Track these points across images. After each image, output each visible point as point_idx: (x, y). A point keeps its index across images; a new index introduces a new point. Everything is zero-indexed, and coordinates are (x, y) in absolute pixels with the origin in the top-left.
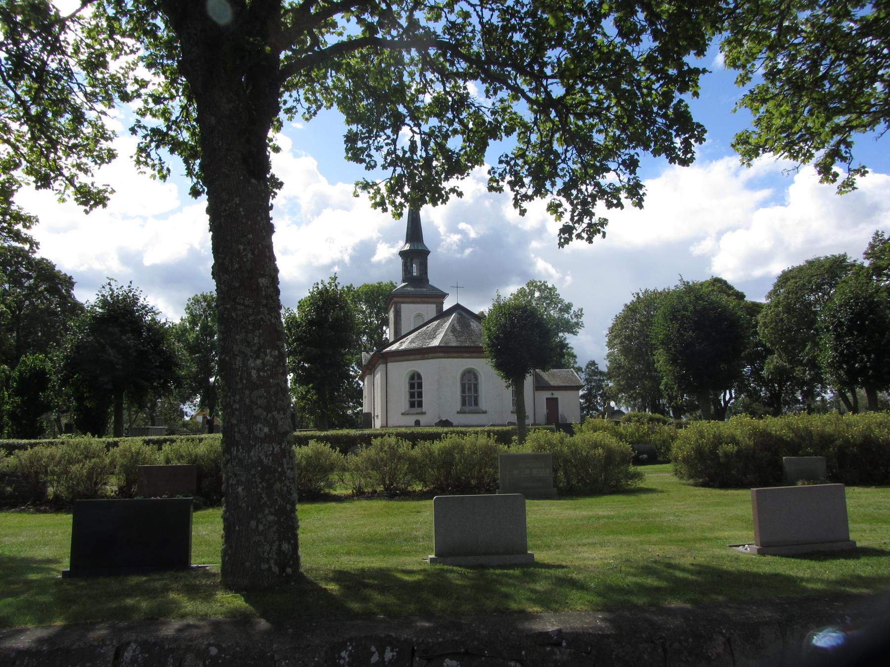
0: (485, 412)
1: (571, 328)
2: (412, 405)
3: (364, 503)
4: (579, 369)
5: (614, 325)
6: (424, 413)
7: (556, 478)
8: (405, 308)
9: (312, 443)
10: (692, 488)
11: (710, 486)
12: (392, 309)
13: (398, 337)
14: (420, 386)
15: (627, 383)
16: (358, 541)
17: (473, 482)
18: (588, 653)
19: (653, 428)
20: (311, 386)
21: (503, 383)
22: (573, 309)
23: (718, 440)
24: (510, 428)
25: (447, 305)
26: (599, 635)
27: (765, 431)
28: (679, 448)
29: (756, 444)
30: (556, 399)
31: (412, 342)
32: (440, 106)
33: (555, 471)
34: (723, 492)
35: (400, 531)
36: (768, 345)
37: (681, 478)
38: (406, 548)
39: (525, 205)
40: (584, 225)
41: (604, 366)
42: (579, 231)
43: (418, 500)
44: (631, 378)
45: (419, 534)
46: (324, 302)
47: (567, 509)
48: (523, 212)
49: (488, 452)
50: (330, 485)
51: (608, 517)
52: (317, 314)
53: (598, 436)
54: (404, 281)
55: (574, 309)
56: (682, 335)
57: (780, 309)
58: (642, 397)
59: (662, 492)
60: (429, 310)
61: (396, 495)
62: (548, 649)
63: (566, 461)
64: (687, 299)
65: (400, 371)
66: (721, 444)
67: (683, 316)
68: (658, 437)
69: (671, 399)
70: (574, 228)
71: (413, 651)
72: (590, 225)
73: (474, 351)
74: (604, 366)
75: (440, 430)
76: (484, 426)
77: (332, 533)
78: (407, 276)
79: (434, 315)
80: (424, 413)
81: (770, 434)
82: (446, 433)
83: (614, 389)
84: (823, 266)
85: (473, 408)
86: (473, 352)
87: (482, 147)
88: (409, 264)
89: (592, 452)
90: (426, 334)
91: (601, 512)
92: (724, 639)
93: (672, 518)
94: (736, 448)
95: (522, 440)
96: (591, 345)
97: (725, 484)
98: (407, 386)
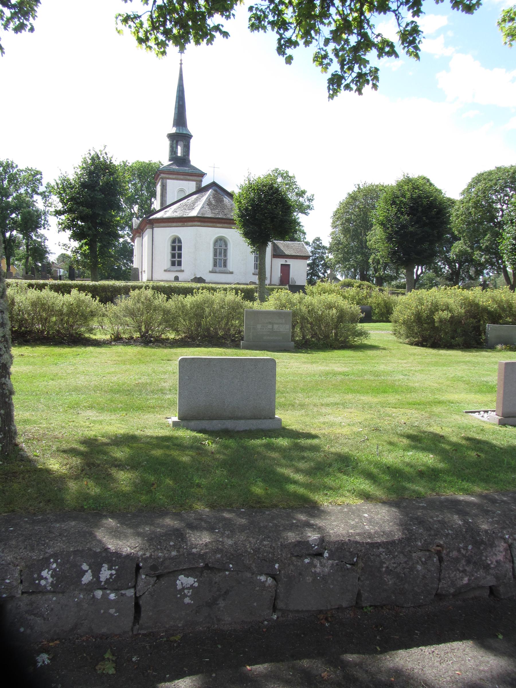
0: (232, 273)
1: (303, 209)
2: (173, 264)
3: (120, 349)
4: (307, 243)
5: (338, 209)
6: (183, 271)
9: (74, 292)
10: (409, 346)
11: (423, 346)
12: (160, 184)
13: (164, 207)
14: (180, 248)
15: (343, 257)
17: (221, 333)
18: (353, 564)
19: (370, 293)
22: (306, 194)
23: (435, 308)
24: (252, 286)
25: (206, 182)
26: (367, 543)
27: (473, 301)
28: (400, 312)
29: (465, 313)
30: (289, 266)
33: (293, 327)
36: (456, 233)
37: (399, 337)
38: (152, 403)
39: (289, 51)
40: (354, 75)
41: (326, 242)
42: (348, 81)
43: (170, 348)
44: (348, 253)
45: (166, 385)
46: (96, 168)
48: (289, 60)
49: (235, 308)
52: (89, 178)
53: (332, 298)
54: (170, 160)
55: (308, 194)
56: (399, 218)
57: (470, 204)
58: (354, 267)
59: (384, 349)
60: (191, 186)
61: (151, 342)
62: (307, 561)
63: (303, 318)
64: (406, 187)
65: (164, 235)
66: (437, 310)
67: (401, 201)
68: (374, 300)
69: (376, 270)
71: (138, 568)
72: (360, 76)
73: (227, 222)
74: (326, 242)
75: (194, 285)
76: (231, 284)
77: (81, 381)
78: (173, 157)
79: (194, 190)
80: (183, 271)
81: (477, 305)
82: (198, 289)
83: (333, 261)
84: (508, 172)
85: (222, 269)
86: (224, 223)
88: (175, 145)
90: (186, 205)
91: (337, 368)
92: (505, 545)
94: (450, 315)
95: (263, 299)
96: (318, 226)
97: (435, 345)
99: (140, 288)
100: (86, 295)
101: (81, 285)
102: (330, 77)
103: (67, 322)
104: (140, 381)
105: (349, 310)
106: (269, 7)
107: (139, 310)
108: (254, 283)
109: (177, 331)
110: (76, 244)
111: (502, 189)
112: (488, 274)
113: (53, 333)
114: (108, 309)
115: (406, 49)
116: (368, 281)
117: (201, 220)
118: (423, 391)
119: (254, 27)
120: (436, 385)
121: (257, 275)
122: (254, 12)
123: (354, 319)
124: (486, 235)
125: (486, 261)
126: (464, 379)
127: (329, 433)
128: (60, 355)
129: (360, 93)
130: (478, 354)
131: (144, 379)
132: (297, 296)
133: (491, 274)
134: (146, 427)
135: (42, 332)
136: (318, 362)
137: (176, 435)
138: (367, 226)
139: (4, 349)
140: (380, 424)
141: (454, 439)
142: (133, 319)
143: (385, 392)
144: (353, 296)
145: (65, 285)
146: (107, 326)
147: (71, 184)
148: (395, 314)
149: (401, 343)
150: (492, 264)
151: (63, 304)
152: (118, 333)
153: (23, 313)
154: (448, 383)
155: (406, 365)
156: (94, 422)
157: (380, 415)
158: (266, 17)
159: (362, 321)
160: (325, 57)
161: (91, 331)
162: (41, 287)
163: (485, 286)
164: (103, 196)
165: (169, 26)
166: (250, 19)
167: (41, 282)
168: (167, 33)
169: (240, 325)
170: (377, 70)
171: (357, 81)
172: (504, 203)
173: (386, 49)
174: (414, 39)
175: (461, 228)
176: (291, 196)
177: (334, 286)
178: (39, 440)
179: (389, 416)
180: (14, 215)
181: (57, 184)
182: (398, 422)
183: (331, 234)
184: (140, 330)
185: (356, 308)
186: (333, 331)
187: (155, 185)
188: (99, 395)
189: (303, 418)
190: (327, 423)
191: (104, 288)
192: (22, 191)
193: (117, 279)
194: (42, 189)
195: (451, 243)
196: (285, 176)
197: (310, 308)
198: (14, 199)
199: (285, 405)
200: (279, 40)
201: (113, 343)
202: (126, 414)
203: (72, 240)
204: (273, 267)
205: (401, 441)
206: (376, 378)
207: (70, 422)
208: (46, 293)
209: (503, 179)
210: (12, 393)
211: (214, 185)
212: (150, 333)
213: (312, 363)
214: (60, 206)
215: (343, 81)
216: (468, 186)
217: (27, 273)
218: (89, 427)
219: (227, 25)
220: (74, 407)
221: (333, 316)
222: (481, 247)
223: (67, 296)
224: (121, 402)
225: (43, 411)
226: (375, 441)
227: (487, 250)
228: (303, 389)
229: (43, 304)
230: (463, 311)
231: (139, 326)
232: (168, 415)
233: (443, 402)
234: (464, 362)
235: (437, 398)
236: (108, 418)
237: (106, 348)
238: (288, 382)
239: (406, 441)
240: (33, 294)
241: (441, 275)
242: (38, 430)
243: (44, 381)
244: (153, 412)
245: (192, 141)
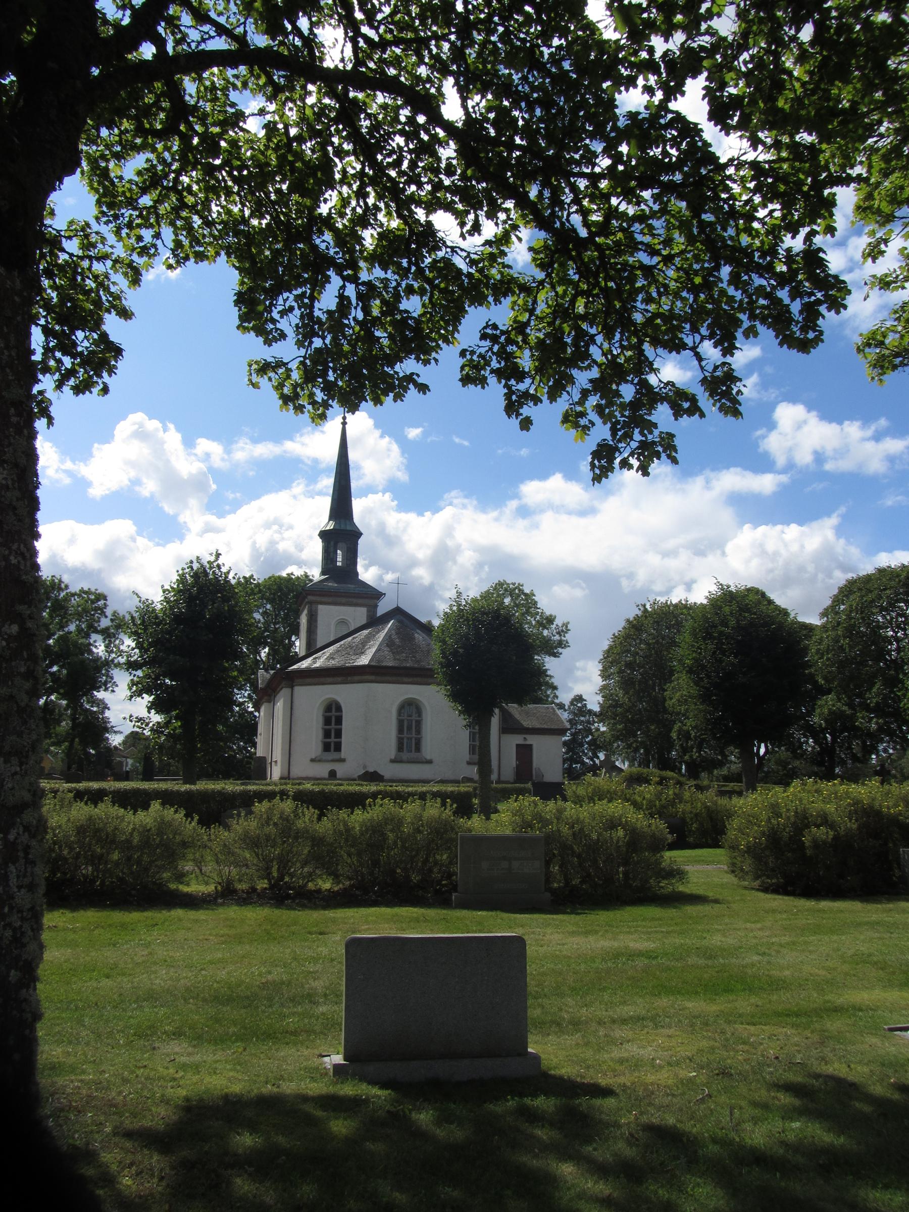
0: (430, 762)
1: (552, 648)
2: (326, 748)
3: (233, 912)
4: (561, 706)
6: (343, 760)
7: (548, 878)
8: (324, 611)
9: (155, 806)
10: (761, 895)
11: (787, 893)
12: (305, 612)
13: (312, 650)
14: (339, 720)
16: (205, 1000)
17: (415, 878)
20: (174, 713)
21: (461, 721)
23: (803, 821)
25: (383, 607)
27: (871, 807)
28: (740, 830)
29: (859, 828)
31: (331, 657)
32: (392, 249)
33: (548, 863)
34: (810, 904)
35: (285, 977)
38: (291, 1022)
40: (634, 445)
41: (594, 703)
46: (201, 589)
47: (573, 933)
48: (526, 424)
49: (441, 834)
50: (180, 877)
51: (650, 955)
53: (616, 808)
55: (559, 622)
59: (716, 901)
61: (288, 897)
64: (727, 610)
65: (311, 700)
66: (808, 826)
67: (721, 633)
68: (688, 808)
69: (685, 750)
70: (617, 449)
73: (421, 675)
74: (594, 703)
77: (161, 978)
79: (364, 621)
80: (343, 760)
81: (878, 813)
85: (413, 755)
87: (455, 315)
88: (332, 549)
89: (607, 834)
90: (351, 647)
93: (756, 958)
94: (831, 833)
95: (488, 811)
96: (580, 678)
97: (810, 892)
98: (321, 720)
99: (270, 796)
100: (176, 812)
101: (166, 790)
102: (595, 448)
103: (139, 862)
104: (270, 977)
105: (646, 829)
106: (491, 349)
107: (268, 838)
108: (470, 780)
109: (336, 876)
110: (156, 718)
111: (892, 605)
112: (885, 751)
113: (112, 882)
114: (213, 837)
115: (718, 405)
116: (672, 770)
117: (375, 673)
118: (800, 985)
119: (466, 380)
120: (822, 972)
121: (474, 764)
122: (468, 357)
123: (657, 845)
124: (874, 684)
125: (880, 729)
126: (875, 959)
127: (633, 1084)
128: (123, 926)
129: (646, 473)
130: (891, 906)
131: (278, 974)
132: (551, 806)
133: (891, 751)
134: (282, 1078)
135: (93, 881)
136: (596, 932)
137: (342, 1093)
138: (665, 674)
139: (30, 933)
140: (729, 1061)
141: (878, 1090)
142: (257, 855)
143: (728, 990)
144: (650, 801)
145: (136, 792)
146: (209, 867)
147: (157, 617)
148: (732, 832)
149: (745, 888)
150: (891, 734)
151: (134, 829)
152: (229, 882)
153: (60, 847)
154: (846, 968)
155: (760, 933)
156: (184, 1067)
157: (727, 1040)
158: (488, 363)
159: (672, 847)
160: (582, 414)
161: (180, 877)
162: (96, 797)
163: (884, 774)
164: (211, 636)
165: (331, 377)
166: (462, 368)
167: (95, 785)
168: (329, 388)
169: (451, 863)
170: (671, 436)
171: (639, 454)
172: (899, 627)
173: (681, 402)
174: (730, 389)
175: (830, 672)
176: (530, 626)
177: (614, 783)
178: (79, 1112)
179: (744, 1043)
180: (55, 668)
181: (133, 618)
182: (763, 1056)
183: (601, 690)
184: (268, 876)
185: (659, 826)
186: (621, 869)
187: (298, 615)
188: (193, 1007)
189: (580, 1050)
190: (627, 1061)
191: (205, 796)
192: (72, 627)
193: (226, 776)
194: (105, 623)
195: (814, 699)
196: (516, 592)
197: (577, 827)
198: (57, 641)
199: (544, 1023)
200: (508, 396)
201: (220, 901)
202: (245, 1049)
203: (153, 711)
204: (504, 750)
205: (774, 1098)
206: (710, 963)
207: (139, 1068)
208: (106, 810)
209: (891, 588)
210: (37, 1016)
211: (398, 613)
212: (287, 879)
213: (587, 933)
214: (136, 655)
215: (617, 454)
216: (834, 601)
217: (69, 768)
218: (174, 1079)
219: (425, 374)
220: (146, 1034)
221: (618, 841)
222: (868, 705)
223: (141, 814)
224: (235, 1023)
225: (87, 1044)
226: (723, 1098)
227: (879, 710)
228: (573, 989)
229: (98, 831)
230: (855, 826)
231: (267, 868)
232: (322, 1050)
233: (842, 1008)
234: (867, 923)
235: (829, 1001)
236: (210, 1058)
237: (207, 912)
238: (544, 974)
239: (785, 1099)
240: (81, 811)
241: (802, 755)
242: (79, 1088)
243: (91, 979)
244: (295, 1044)
245: (361, 541)
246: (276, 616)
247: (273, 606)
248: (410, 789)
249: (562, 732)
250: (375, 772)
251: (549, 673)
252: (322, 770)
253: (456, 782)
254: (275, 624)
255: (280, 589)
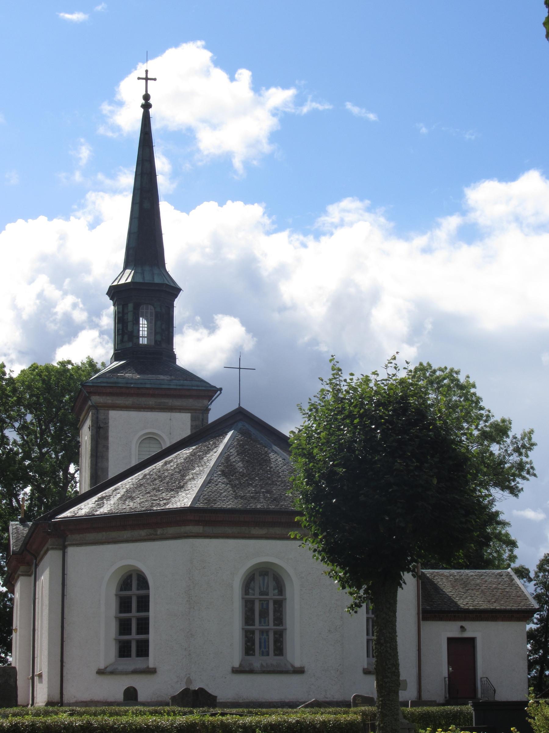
0: (300, 671)
1: (507, 477)
2: (124, 651)
4: (522, 573)
6: (152, 671)
12: (88, 423)
13: (100, 483)
14: (144, 603)
25: (217, 410)
31: (128, 496)
55: (516, 431)
65: (95, 568)
80: (152, 671)
85: (272, 660)
88: (130, 317)
108: (368, 701)
117: (203, 520)
187: (77, 431)
211: (240, 418)
246: (42, 432)
247: (37, 417)
248: (248, 719)
249: (525, 615)
250: (201, 691)
251: (502, 517)
252: (113, 689)
253: (346, 704)
254: (40, 447)
255: (48, 386)
